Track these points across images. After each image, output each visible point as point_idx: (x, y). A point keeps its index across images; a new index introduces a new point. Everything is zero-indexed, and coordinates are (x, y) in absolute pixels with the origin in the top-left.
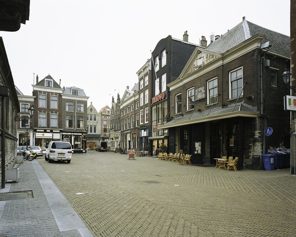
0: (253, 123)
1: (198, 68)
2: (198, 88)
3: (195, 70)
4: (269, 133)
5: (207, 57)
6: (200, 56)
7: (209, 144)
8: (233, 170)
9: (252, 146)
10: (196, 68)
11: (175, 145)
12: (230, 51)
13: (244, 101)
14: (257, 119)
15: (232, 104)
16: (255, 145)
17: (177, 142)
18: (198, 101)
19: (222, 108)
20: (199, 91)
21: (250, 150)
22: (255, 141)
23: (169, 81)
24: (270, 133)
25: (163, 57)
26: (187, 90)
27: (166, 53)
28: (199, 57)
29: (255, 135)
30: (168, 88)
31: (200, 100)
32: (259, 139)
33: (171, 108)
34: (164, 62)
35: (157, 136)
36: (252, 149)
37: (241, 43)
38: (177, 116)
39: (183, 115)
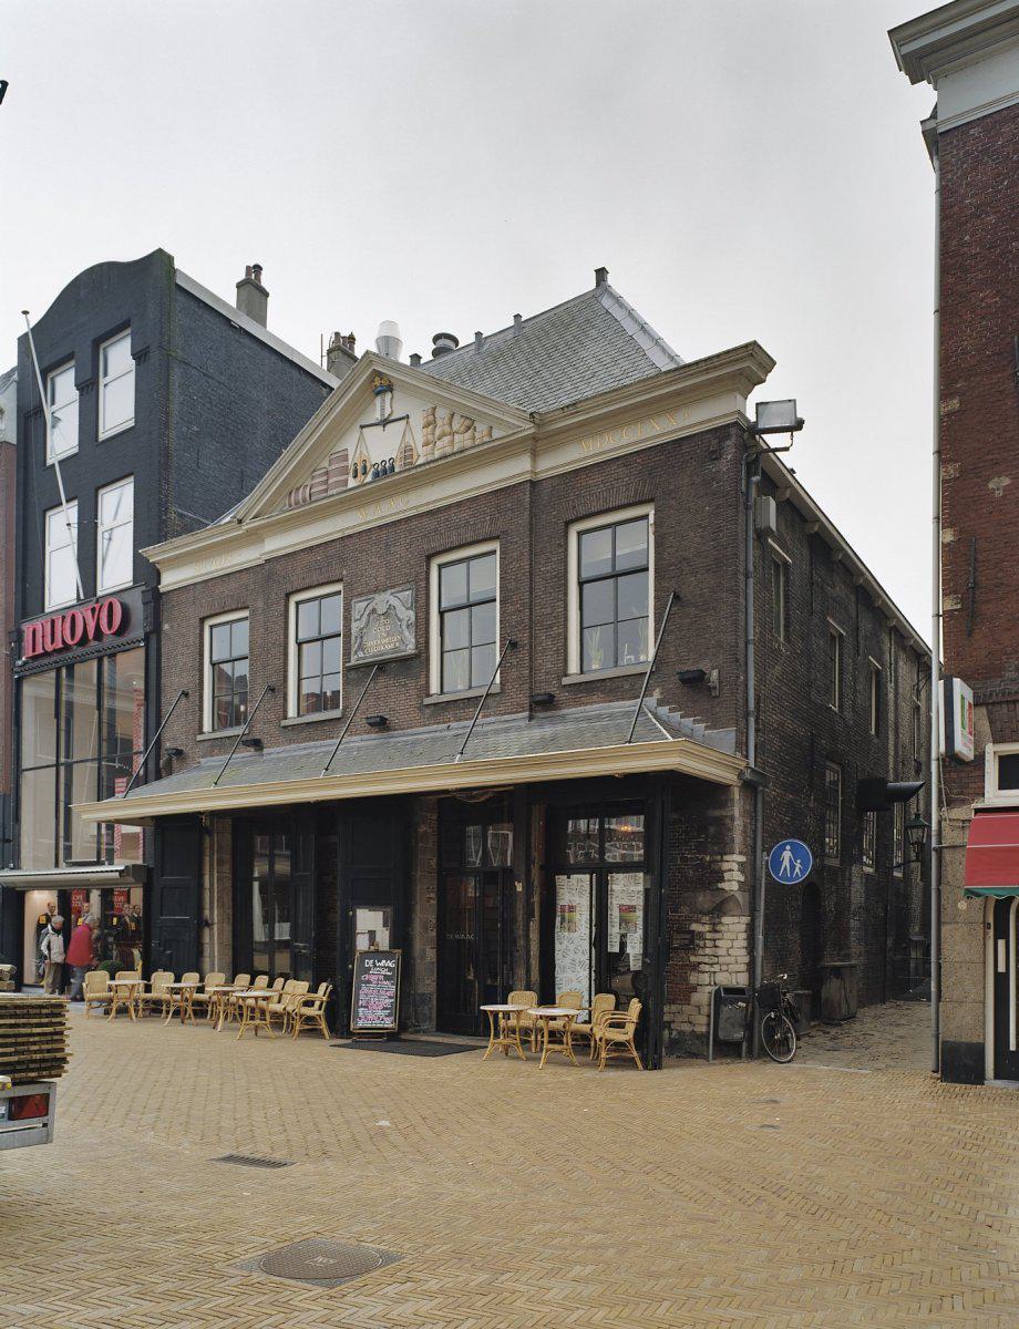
0: (717, 813)
1: (369, 478)
2: (370, 592)
3: (352, 483)
4: (792, 872)
5: (430, 424)
6: (383, 409)
7: (434, 921)
8: (319, 1034)
9: (708, 936)
10: (355, 477)
11: (203, 923)
12: (586, 411)
13: (657, 690)
14: (736, 794)
15: (586, 704)
16: (719, 928)
17: (212, 903)
18: (369, 666)
19: (531, 718)
20: (374, 611)
21: (693, 959)
22: (719, 910)
23: (151, 527)
24: (797, 870)
25: (106, 375)
26: (288, 596)
27: (139, 356)
28: (377, 416)
29: (727, 876)
30: (146, 573)
31: (382, 667)
32: (739, 896)
33: (170, 696)
34: (118, 408)
35: (57, 865)
36: (708, 951)
37: (593, 397)
38: (217, 745)
39: (257, 744)
